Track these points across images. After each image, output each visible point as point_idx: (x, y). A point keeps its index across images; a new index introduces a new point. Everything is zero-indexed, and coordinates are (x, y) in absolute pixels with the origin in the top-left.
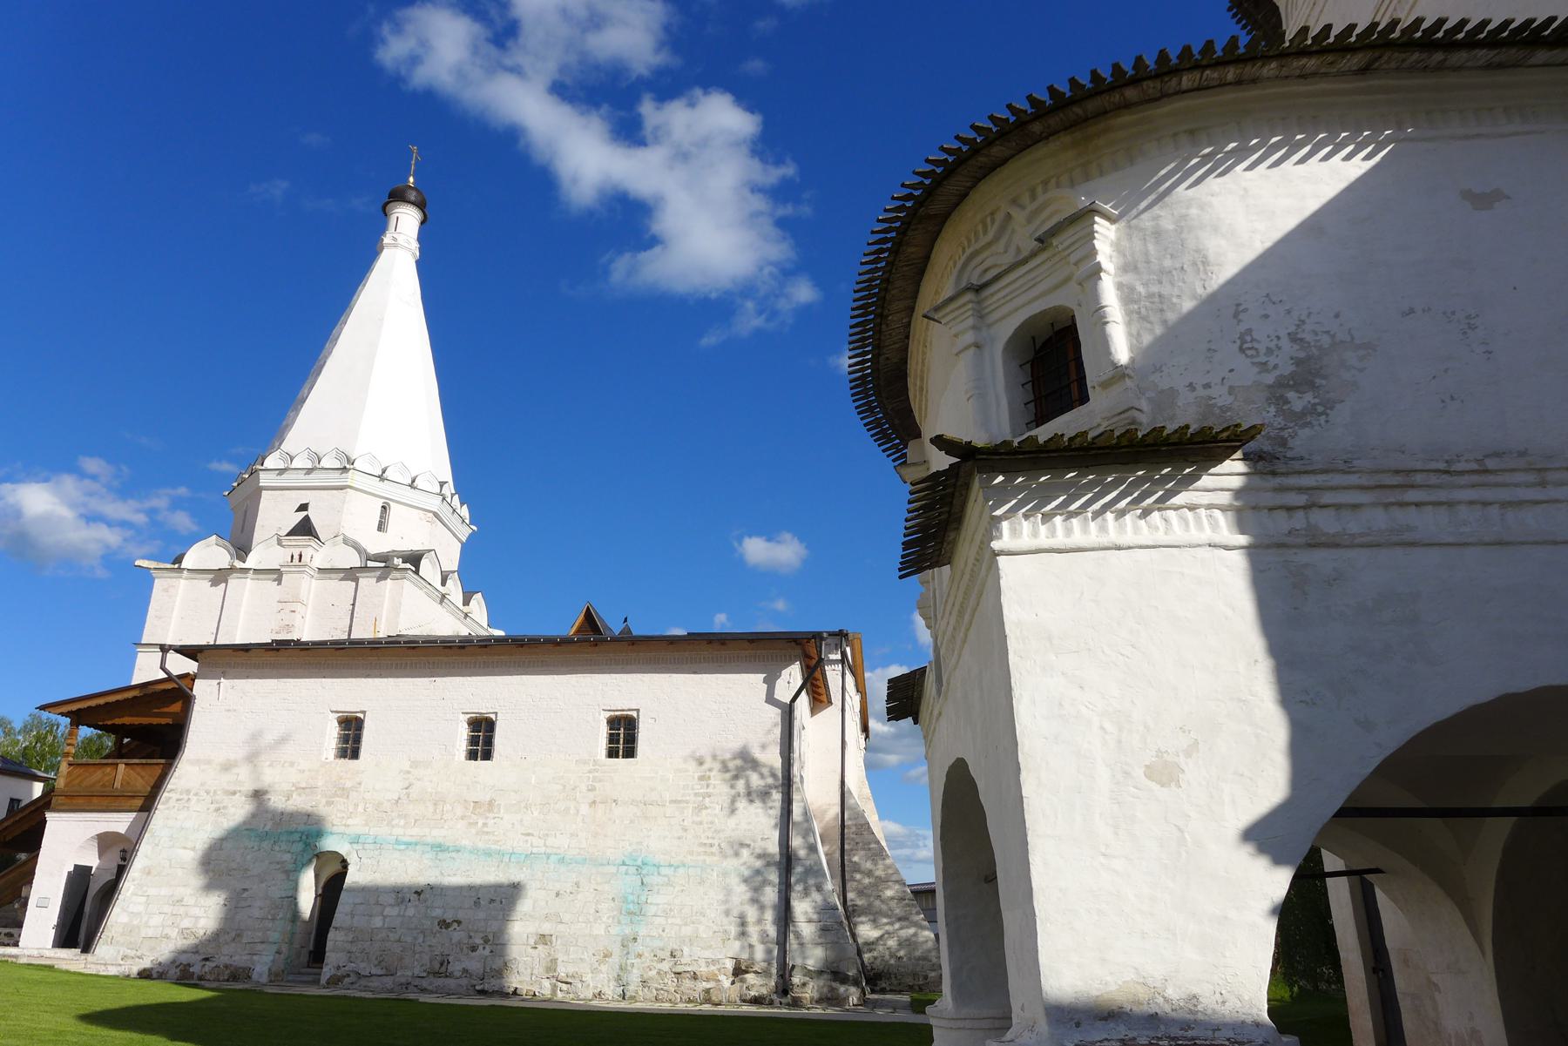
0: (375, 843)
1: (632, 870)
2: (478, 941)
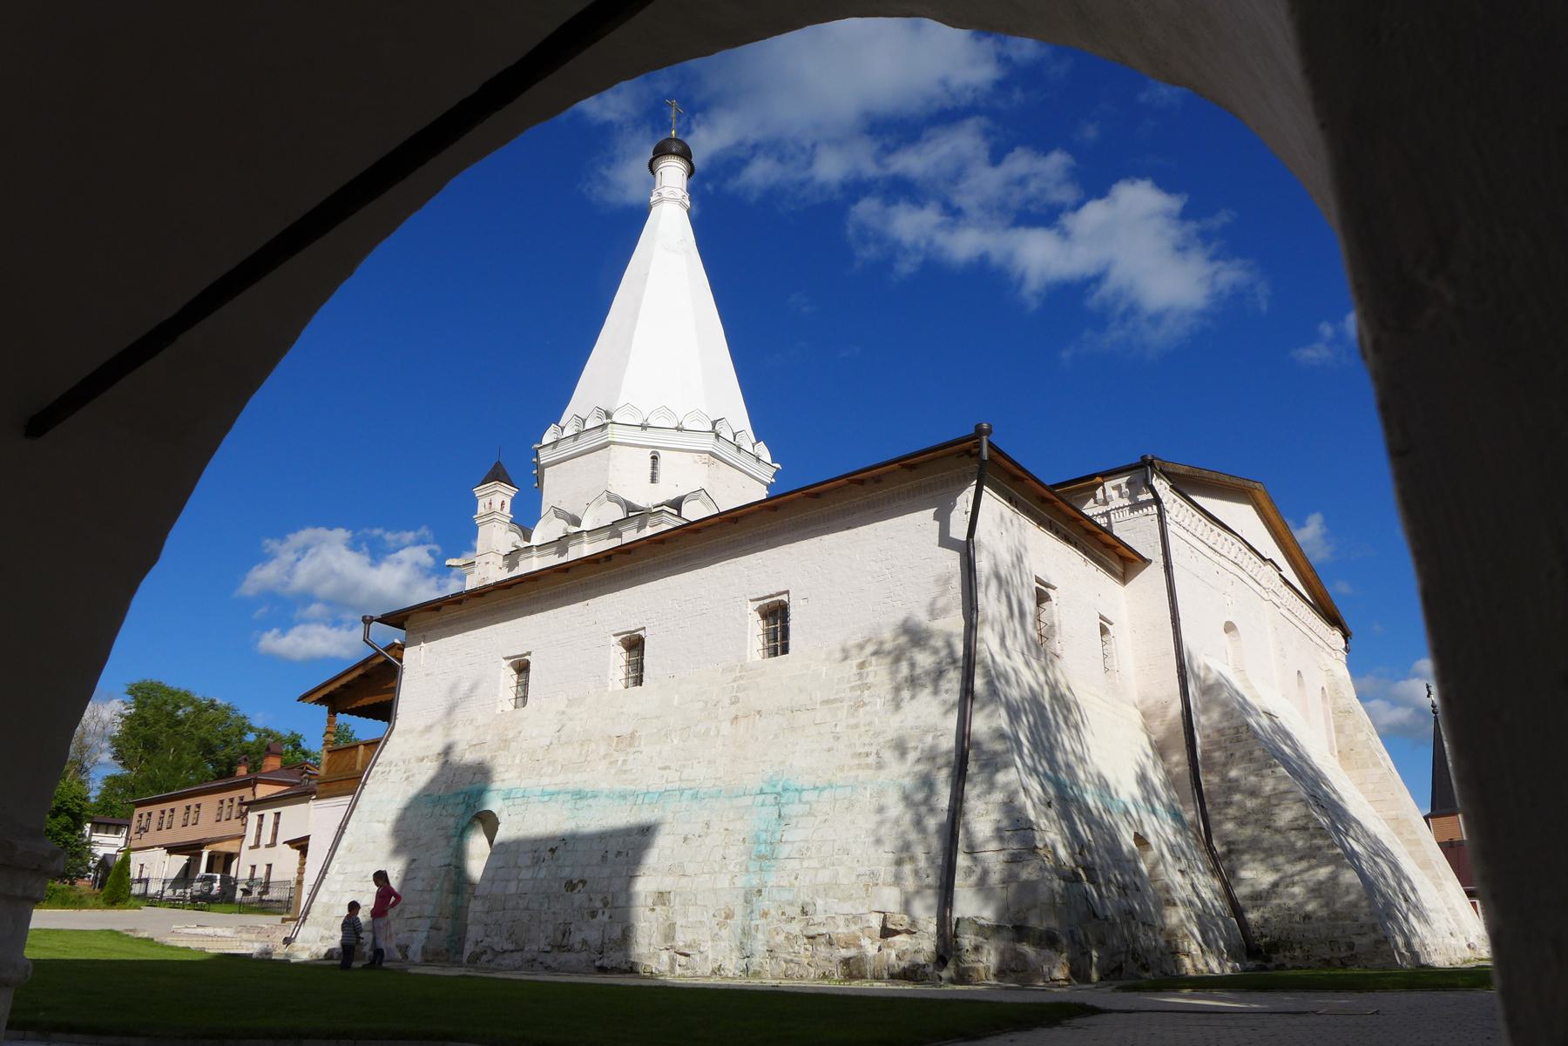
0: (523, 796)
1: (770, 799)
2: (598, 904)
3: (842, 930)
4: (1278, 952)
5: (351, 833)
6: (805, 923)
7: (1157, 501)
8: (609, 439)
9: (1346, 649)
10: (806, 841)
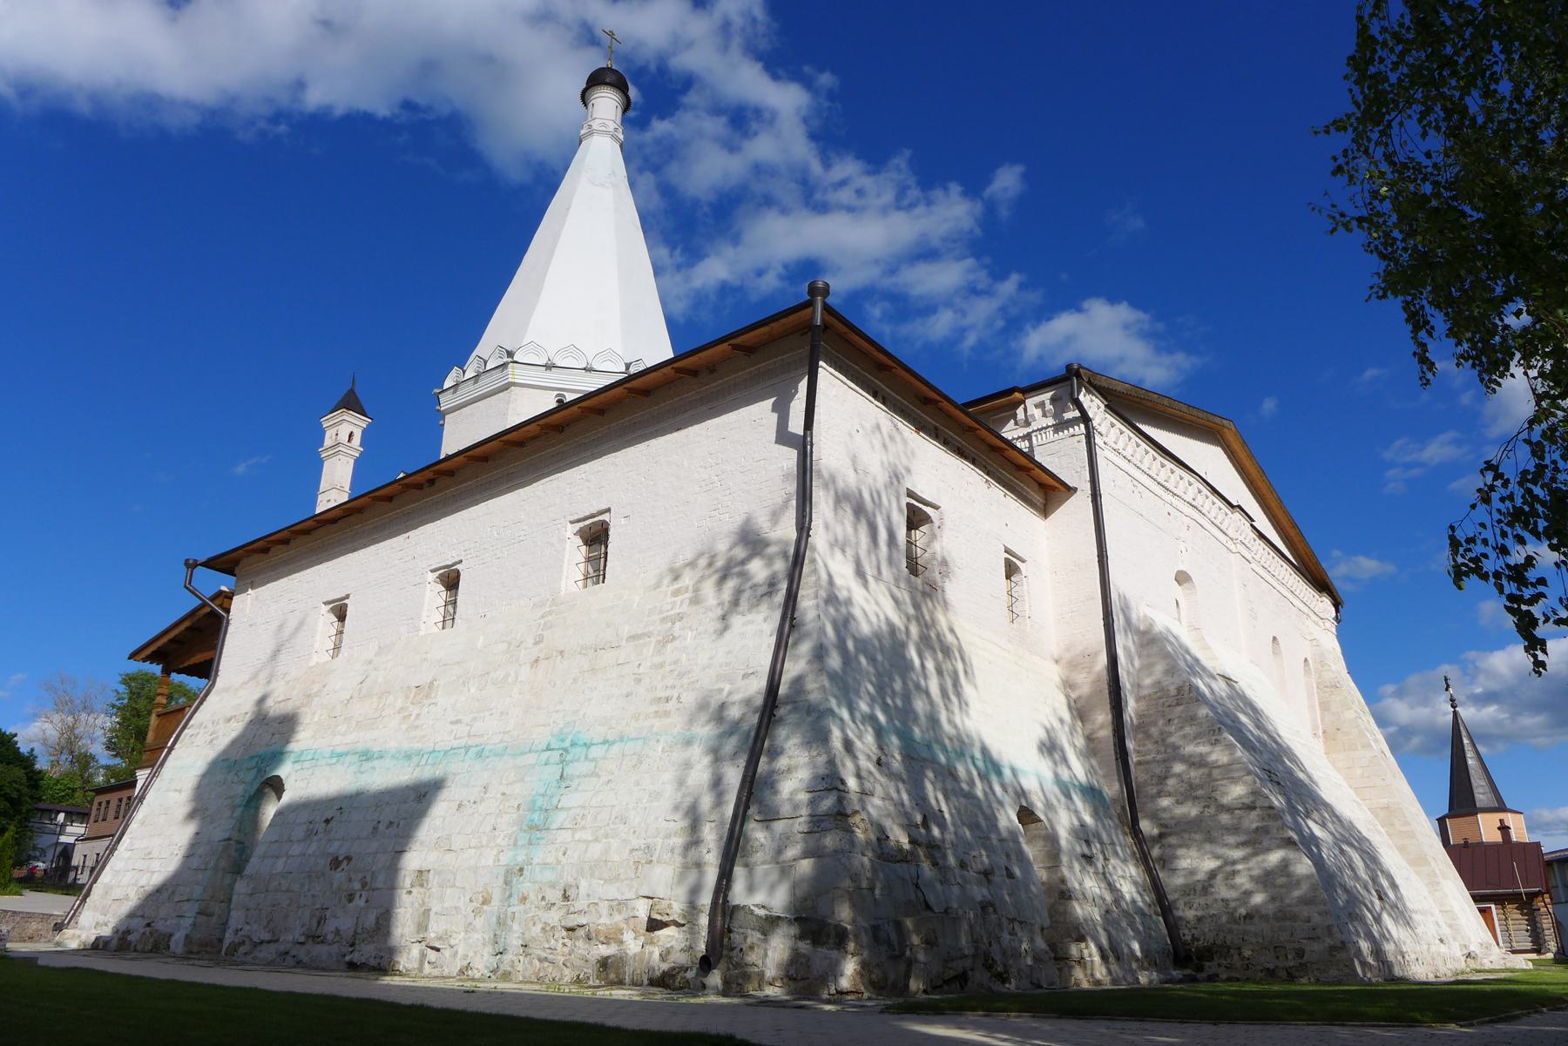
0: (313, 759)
1: (555, 756)
2: (357, 886)
3: (604, 920)
4: (1212, 959)
5: (148, 805)
6: (565, 910)
7: (1085, 419)
8: (510, 380)
9: (1336, 618)
10: (583, 807)
